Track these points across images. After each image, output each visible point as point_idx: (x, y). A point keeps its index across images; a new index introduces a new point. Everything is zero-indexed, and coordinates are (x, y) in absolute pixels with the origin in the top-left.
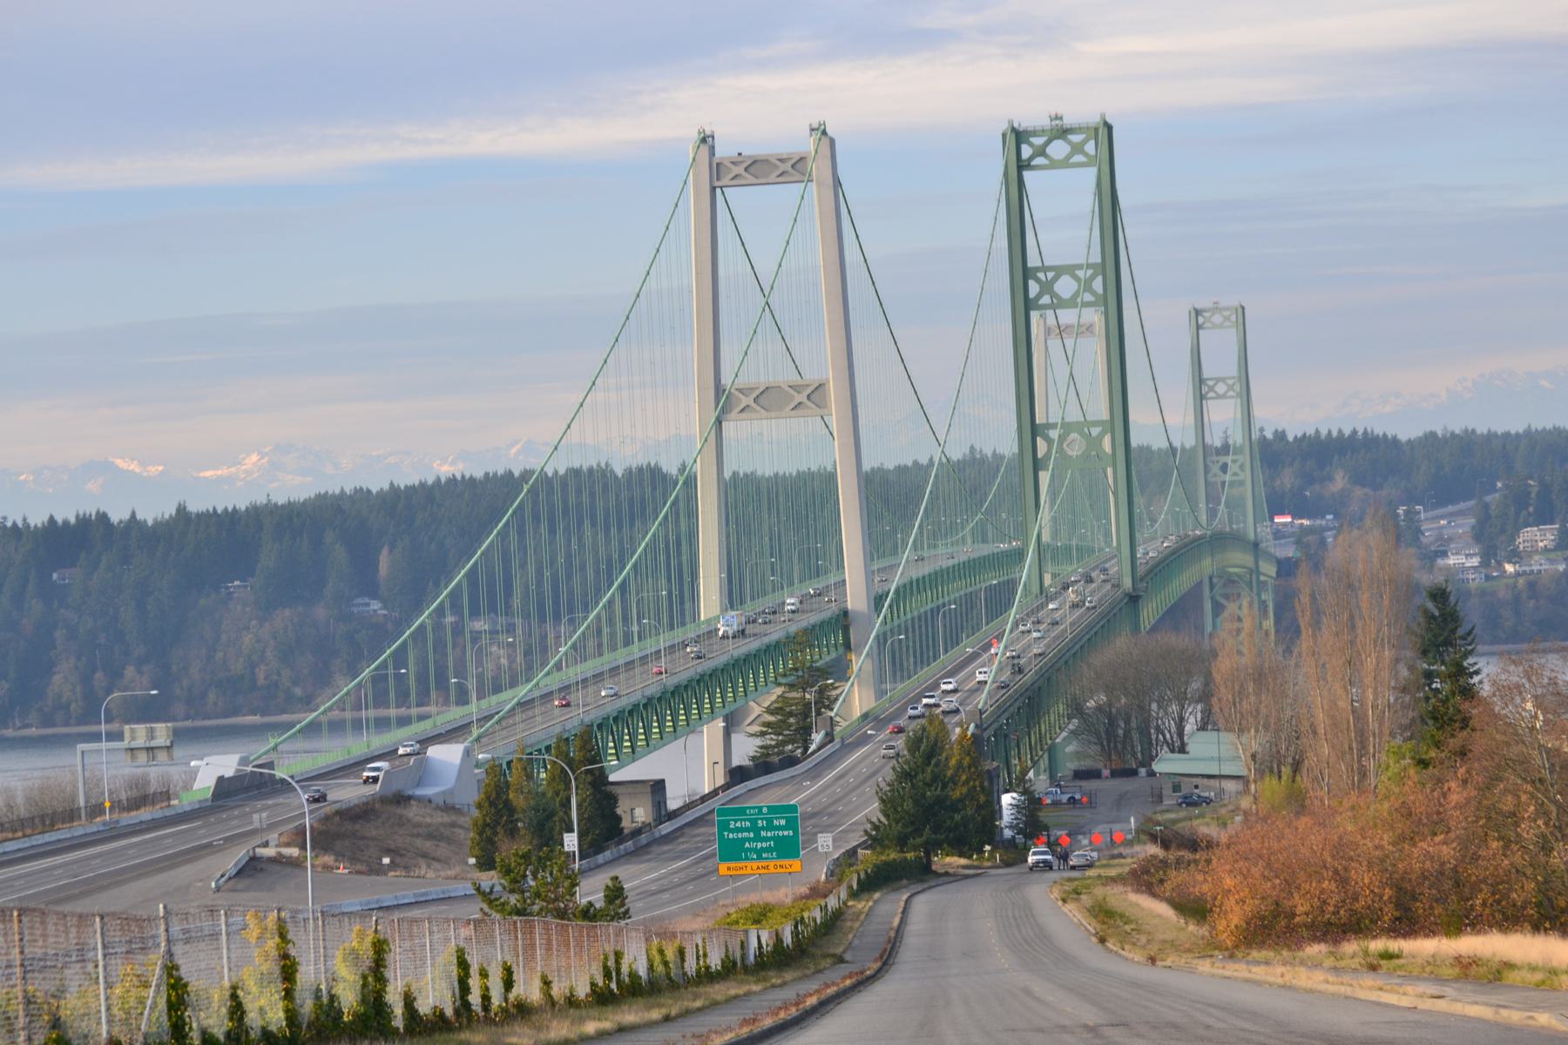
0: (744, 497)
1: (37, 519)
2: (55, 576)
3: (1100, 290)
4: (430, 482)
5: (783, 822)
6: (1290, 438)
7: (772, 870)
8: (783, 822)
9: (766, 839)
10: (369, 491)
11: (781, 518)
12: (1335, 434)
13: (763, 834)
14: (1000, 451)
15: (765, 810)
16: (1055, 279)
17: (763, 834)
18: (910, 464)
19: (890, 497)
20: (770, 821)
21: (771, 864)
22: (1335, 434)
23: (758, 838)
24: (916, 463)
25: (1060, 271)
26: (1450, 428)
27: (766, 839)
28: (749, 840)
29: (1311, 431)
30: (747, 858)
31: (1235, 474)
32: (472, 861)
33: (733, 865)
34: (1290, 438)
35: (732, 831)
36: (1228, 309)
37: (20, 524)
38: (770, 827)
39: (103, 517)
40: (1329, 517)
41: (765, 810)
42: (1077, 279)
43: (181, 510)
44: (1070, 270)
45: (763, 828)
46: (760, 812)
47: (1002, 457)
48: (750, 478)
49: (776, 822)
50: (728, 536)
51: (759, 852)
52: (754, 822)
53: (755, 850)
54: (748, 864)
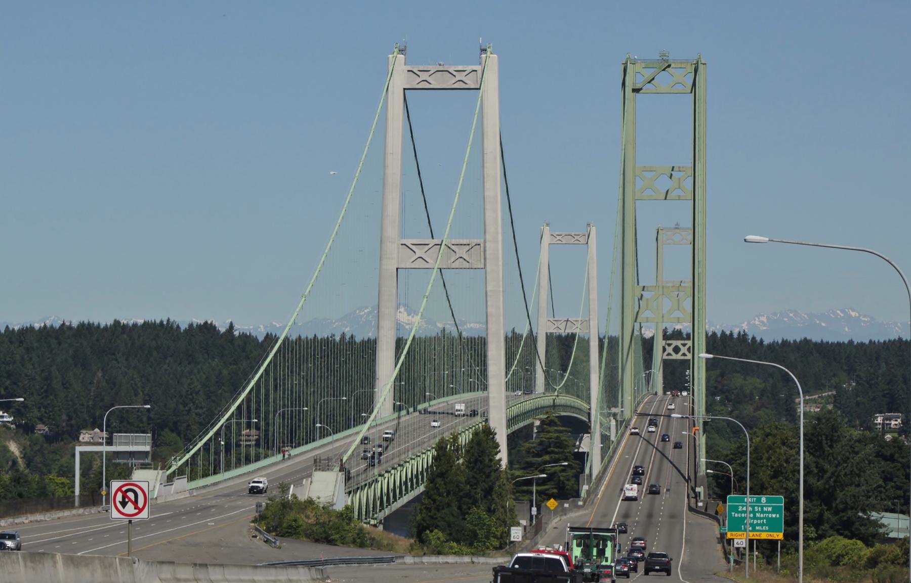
5: (770, 509)
8: (770, 509)
9: (760, 518)
23: (755, 518)
38: (762, 512)
45: (758, 512)
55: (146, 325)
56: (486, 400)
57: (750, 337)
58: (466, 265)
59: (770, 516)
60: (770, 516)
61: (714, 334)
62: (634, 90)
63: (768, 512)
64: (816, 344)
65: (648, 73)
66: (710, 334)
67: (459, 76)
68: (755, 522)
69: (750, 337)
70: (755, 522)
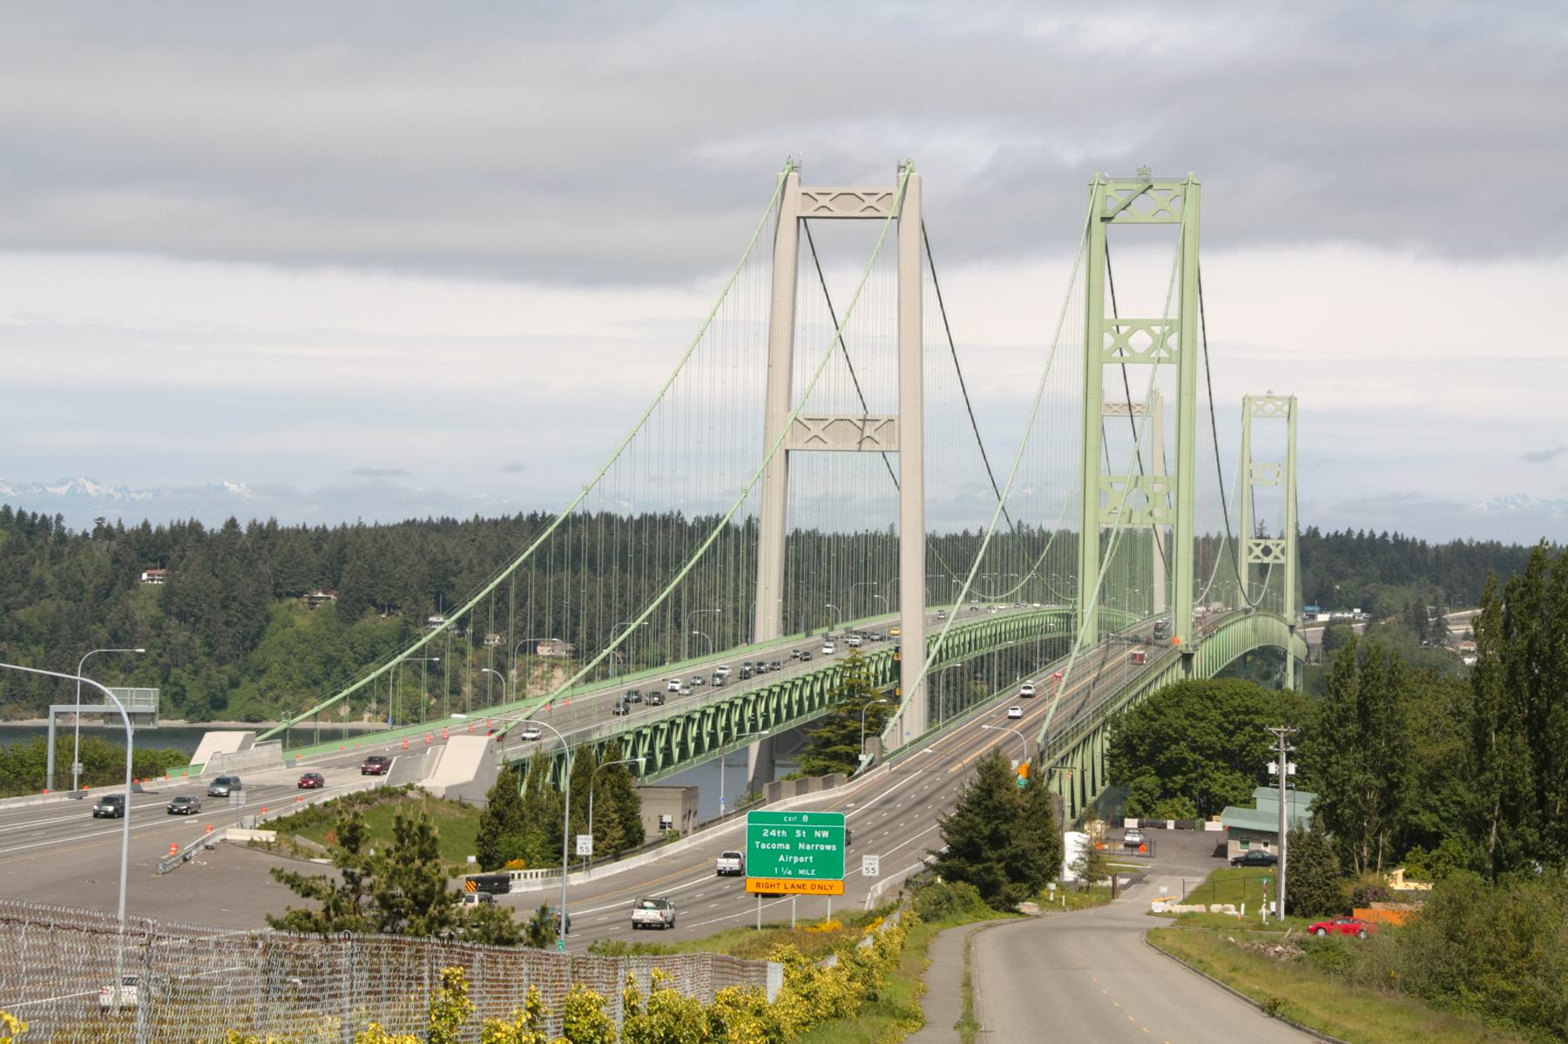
0: (805, 552)
1: (131, 523)
2: (145, 576)
3: (1175, 348)
4: (512, 518)
5: (826, 834)
6: (1323, 535)
7: (808, 890)
8: (826, 834)
9: (804, 853)
10: (455, 522)
11: (842, 573)
12: (1366, 534)
13: (801, 846)
14: (1046, 528)
15: (805, 818)
16: (1129, 334)
17: (801, 846)
18: (960, 533)
19: (950, 559)
20: (810, 832)
21: (809, 883)
22: (1366, 534)
23: (795, 851)
24: (966, 533)
25: (1135, 325)
26: (1476, 539)
27: (804, 853)
28: (784, 852)
29: (1343, 531)
30: (780, 874)
31: (1276, 557)
32: (472, 859)
33: (763, 880)
34: (1323, 535)
35: (764, 840)
36: (1280, 399)
37: (115, 526)
38: (810, 839)
39: (195, 527)
40: (1357, 611)
41: (805, 818)
42: (1151, 333)
43: (273, 523)
44: (1146, 325)
45: (801, 839)
46: (800, 820)
47: (1048, 535)
48: (813, 536)
49: (817, 834)
50: (786, 585)
51: (795, 868)
52: (791, 831)
53: (790, 865)
54: (782, 881)
55: (1457, 547)
56: (898, 625)
57: (15, 513)
58: (821, 446)
59: (822, 847)
60: (822, 847)
61: (535, 515)
62: (1103, 219)
63: (822, 841)
64: (495, 523)
65: (1121, 199)
66: (1304, 532)
67: (823, 200)
68: (796, 860)
69: (15, 513)
70: (796, 860)
